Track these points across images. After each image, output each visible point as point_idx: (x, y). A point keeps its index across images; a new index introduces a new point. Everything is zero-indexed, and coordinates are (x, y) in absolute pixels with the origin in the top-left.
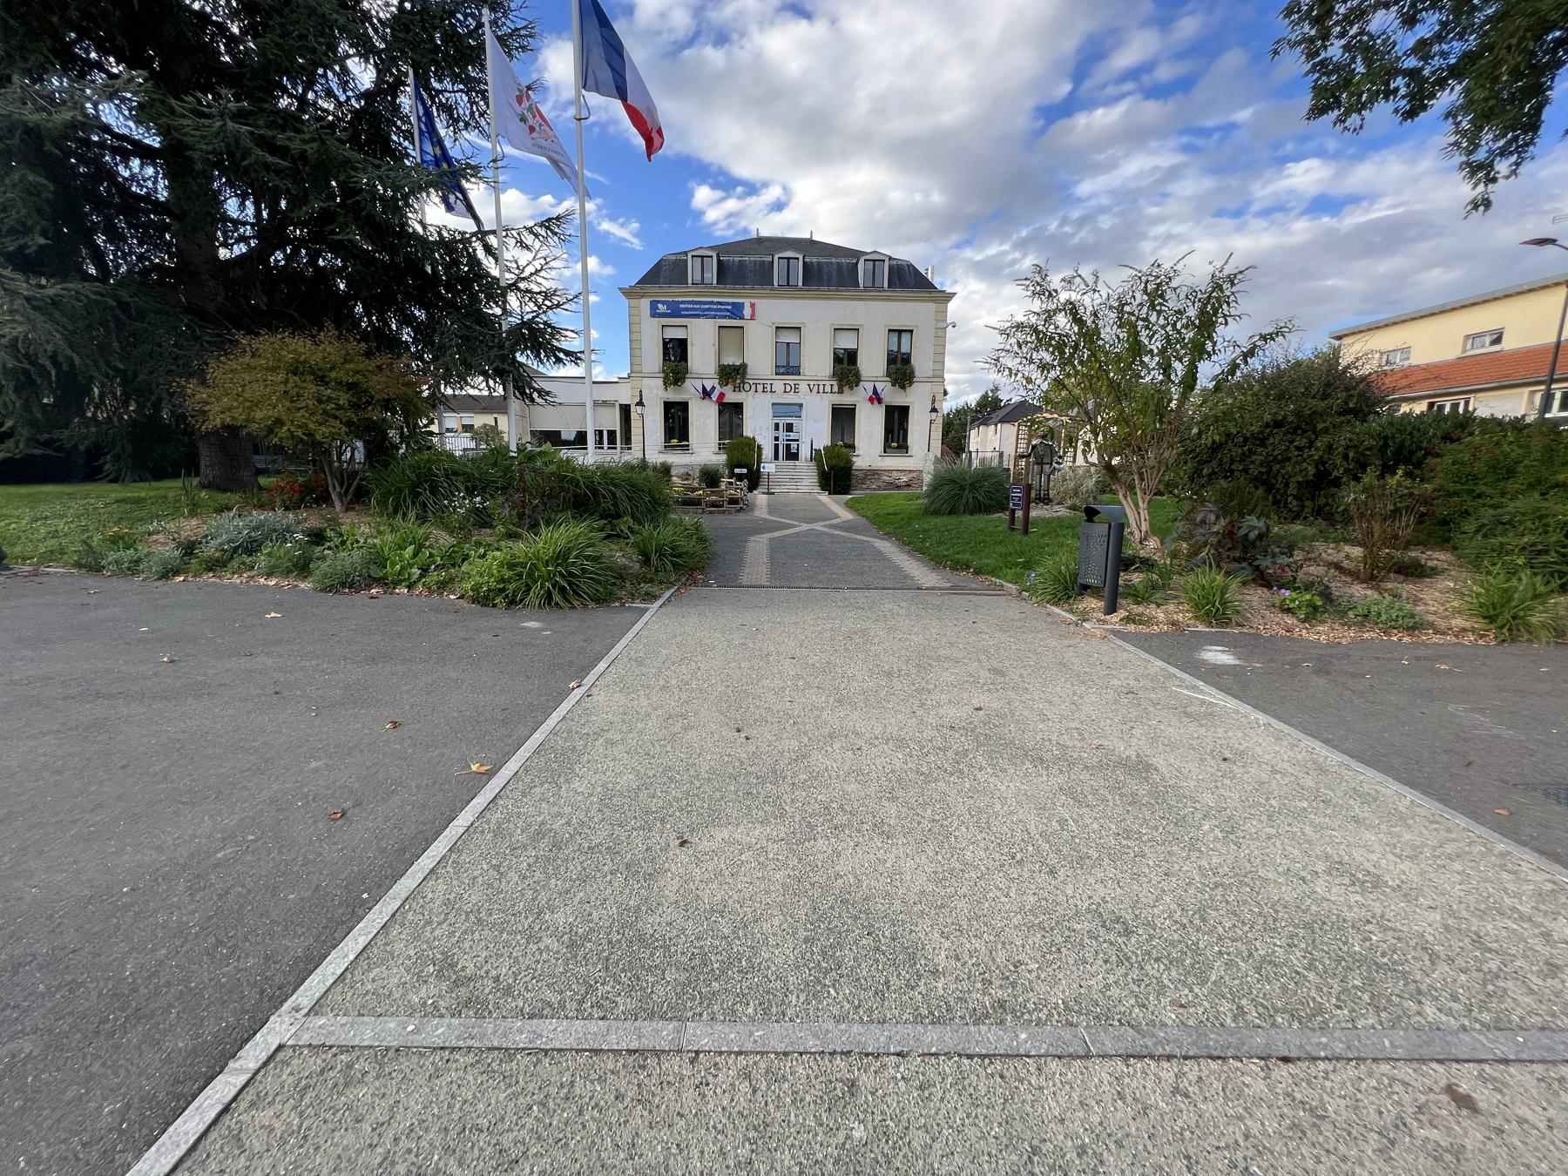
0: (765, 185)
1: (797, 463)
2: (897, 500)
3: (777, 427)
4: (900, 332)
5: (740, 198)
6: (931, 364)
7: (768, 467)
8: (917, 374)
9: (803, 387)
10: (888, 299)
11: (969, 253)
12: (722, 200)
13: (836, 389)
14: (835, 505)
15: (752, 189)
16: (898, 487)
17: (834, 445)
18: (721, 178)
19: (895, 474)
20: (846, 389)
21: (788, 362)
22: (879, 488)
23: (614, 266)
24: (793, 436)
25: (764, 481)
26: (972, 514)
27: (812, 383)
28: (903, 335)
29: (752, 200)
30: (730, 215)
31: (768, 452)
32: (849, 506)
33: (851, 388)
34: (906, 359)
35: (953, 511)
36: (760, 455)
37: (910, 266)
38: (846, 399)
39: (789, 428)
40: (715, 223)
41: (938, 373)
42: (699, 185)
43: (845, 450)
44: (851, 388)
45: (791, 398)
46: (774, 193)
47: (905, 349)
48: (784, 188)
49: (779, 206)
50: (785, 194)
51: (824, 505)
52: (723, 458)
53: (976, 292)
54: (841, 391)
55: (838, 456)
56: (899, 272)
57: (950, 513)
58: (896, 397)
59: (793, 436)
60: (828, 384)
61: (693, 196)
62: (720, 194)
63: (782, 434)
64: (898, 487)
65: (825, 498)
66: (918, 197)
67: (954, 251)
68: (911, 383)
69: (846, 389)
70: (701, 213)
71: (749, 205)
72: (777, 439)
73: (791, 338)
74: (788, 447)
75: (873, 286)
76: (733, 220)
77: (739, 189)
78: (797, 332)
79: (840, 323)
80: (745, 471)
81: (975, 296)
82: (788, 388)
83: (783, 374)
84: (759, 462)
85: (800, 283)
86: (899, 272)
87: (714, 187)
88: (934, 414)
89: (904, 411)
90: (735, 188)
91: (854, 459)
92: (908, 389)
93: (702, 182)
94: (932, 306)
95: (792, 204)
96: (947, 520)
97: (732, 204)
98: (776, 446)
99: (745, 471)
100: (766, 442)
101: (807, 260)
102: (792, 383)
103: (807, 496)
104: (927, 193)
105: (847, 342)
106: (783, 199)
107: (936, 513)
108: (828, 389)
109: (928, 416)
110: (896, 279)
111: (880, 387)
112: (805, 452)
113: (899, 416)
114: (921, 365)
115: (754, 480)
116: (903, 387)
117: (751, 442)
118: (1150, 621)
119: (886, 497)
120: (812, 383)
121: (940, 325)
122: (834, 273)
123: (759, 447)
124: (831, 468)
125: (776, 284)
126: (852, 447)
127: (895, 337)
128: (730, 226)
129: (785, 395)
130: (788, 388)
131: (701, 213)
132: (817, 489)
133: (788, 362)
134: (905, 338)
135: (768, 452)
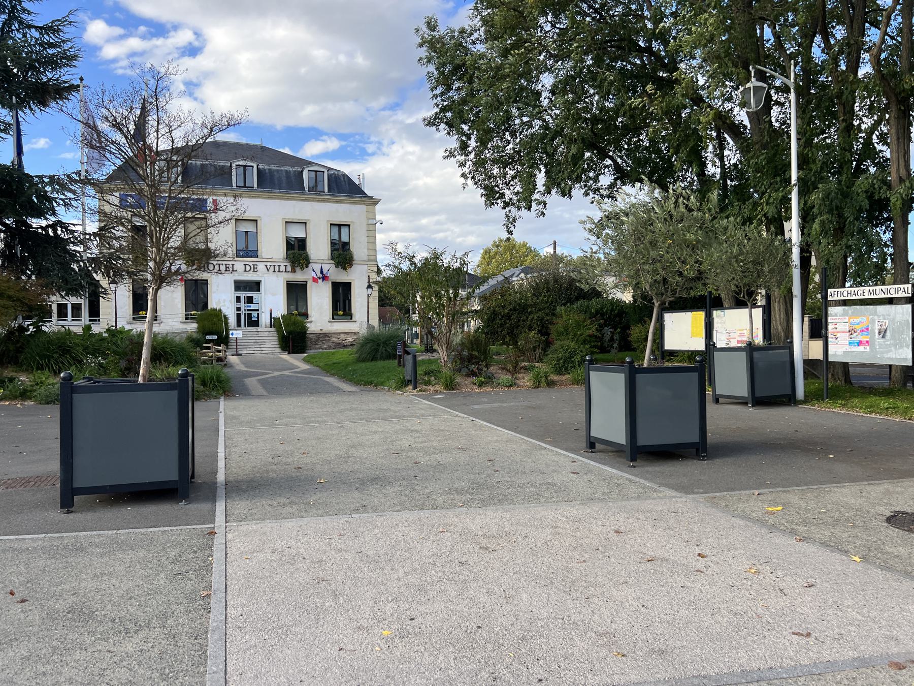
0: (176, 27)
1: (259, 329)
2: (343, 355)
3: (238, 299)
4: (340, 226)
5: (143, 37)
6: (366, 251)
7: (236, 334)
8: (355, 257)
9: (261, 267)
10: (328, 201)
11: (400, 116)
12: (121, 37)
13: (289, 269)
14: (296, 361)
15: (158, 29)
16: (345, 346)
17: (290, 313)
18: (117, 14)
19: (342, 335)
20: (298, 269)
21: (247, 247)
22: (330, 347)
23: (45, 137)
24: (253, 306)
25: (233, 344)
26: (384, 360)
27: (268, 264)
28: (342, 227)
29: (159, 42)
30: (133, 54)
31: (232, 321)
32: (305, 360)
33: (302, 269)
34: (346, 245)
35: (374, 359)
36: (227, 323)
37: (345, 175)
38: (299, 276)
39: (250, 300)
40: (115, 60)
41: (372, 258)
42: (92, 19)
43: (299, 318)
44: (302, 269)
45: (251, 277)
46: (184, 37)
47: (345, 238)
48: (197, 34)
49: (192, 51)
50: (197, 39)
51: (286, 361)
52: (193, 326)
53: (412, 153)
54: (293, 271)
55: (295, 323)
56: (336, 181)
57: (372, 360)
58: (342, 277)
59: (253, 306)
60: (282, 265)
61: (84, 30)
62: (118, 31)
63: (243, 305)
64: (345, 346)
65: (285, 356)
66: (342, 58)
67: (387, 113)
68: (351, 265)
69: (298, 269)
70: (97, 48)
71: (157, 47)
72: (238, 309)
73: (250, 228)
74: (249, 316)
75: (314, 189)
76: (137, 59)
77: (142, 29)
78: (254, 224)
79: (291, 217)
80: (215, 337)
81: (410, 157)
82: (248, 268)
83: (243, 256)
84: (227, 330)
85: (255, 186)
86: (336, 181)
87: (111, 22)
88: (370, 290)
89: (347, 286)
90: (137, 28)
91: (308, 325)
92: (349, 270)
93: (96, 16)
94: (363, 208)
95: (206, 50)
96: (373, 363)
97: (134, 43)
98: (239, 316)
99: (215, 337)
100: (230, 311)
101: (260, 167)
102: (251, 264)
103: (272, 356)
104: (350, 55)
105: (297, 232)
106: (196, 44)
107: (364, 360)
108: (283, 269)
109: (365, 292)
110: (334, 185)
111: (326, 268)
112: (265, 320)
113: (343, 290)
114: (358, 250)
115: (224, 340)
116: (345, 268)
117: (218, 313)
118: (427, 390)
119: (333, 354)
120: (268, 264)
121: (371, 222)
122: (284, 179)
123: (225, 316)
124: (289, 333)
125: (234, 185)
126: (306, 315)
127: (336, 229)
128: (132, 66)
129: (246, 274)
130: (248, 268)
131: (97, 48)
132: (278, 350)
133: (247, 247)
134: (344, 230)
135: (232, 321)
